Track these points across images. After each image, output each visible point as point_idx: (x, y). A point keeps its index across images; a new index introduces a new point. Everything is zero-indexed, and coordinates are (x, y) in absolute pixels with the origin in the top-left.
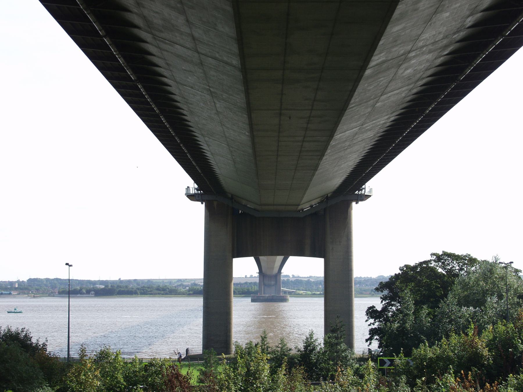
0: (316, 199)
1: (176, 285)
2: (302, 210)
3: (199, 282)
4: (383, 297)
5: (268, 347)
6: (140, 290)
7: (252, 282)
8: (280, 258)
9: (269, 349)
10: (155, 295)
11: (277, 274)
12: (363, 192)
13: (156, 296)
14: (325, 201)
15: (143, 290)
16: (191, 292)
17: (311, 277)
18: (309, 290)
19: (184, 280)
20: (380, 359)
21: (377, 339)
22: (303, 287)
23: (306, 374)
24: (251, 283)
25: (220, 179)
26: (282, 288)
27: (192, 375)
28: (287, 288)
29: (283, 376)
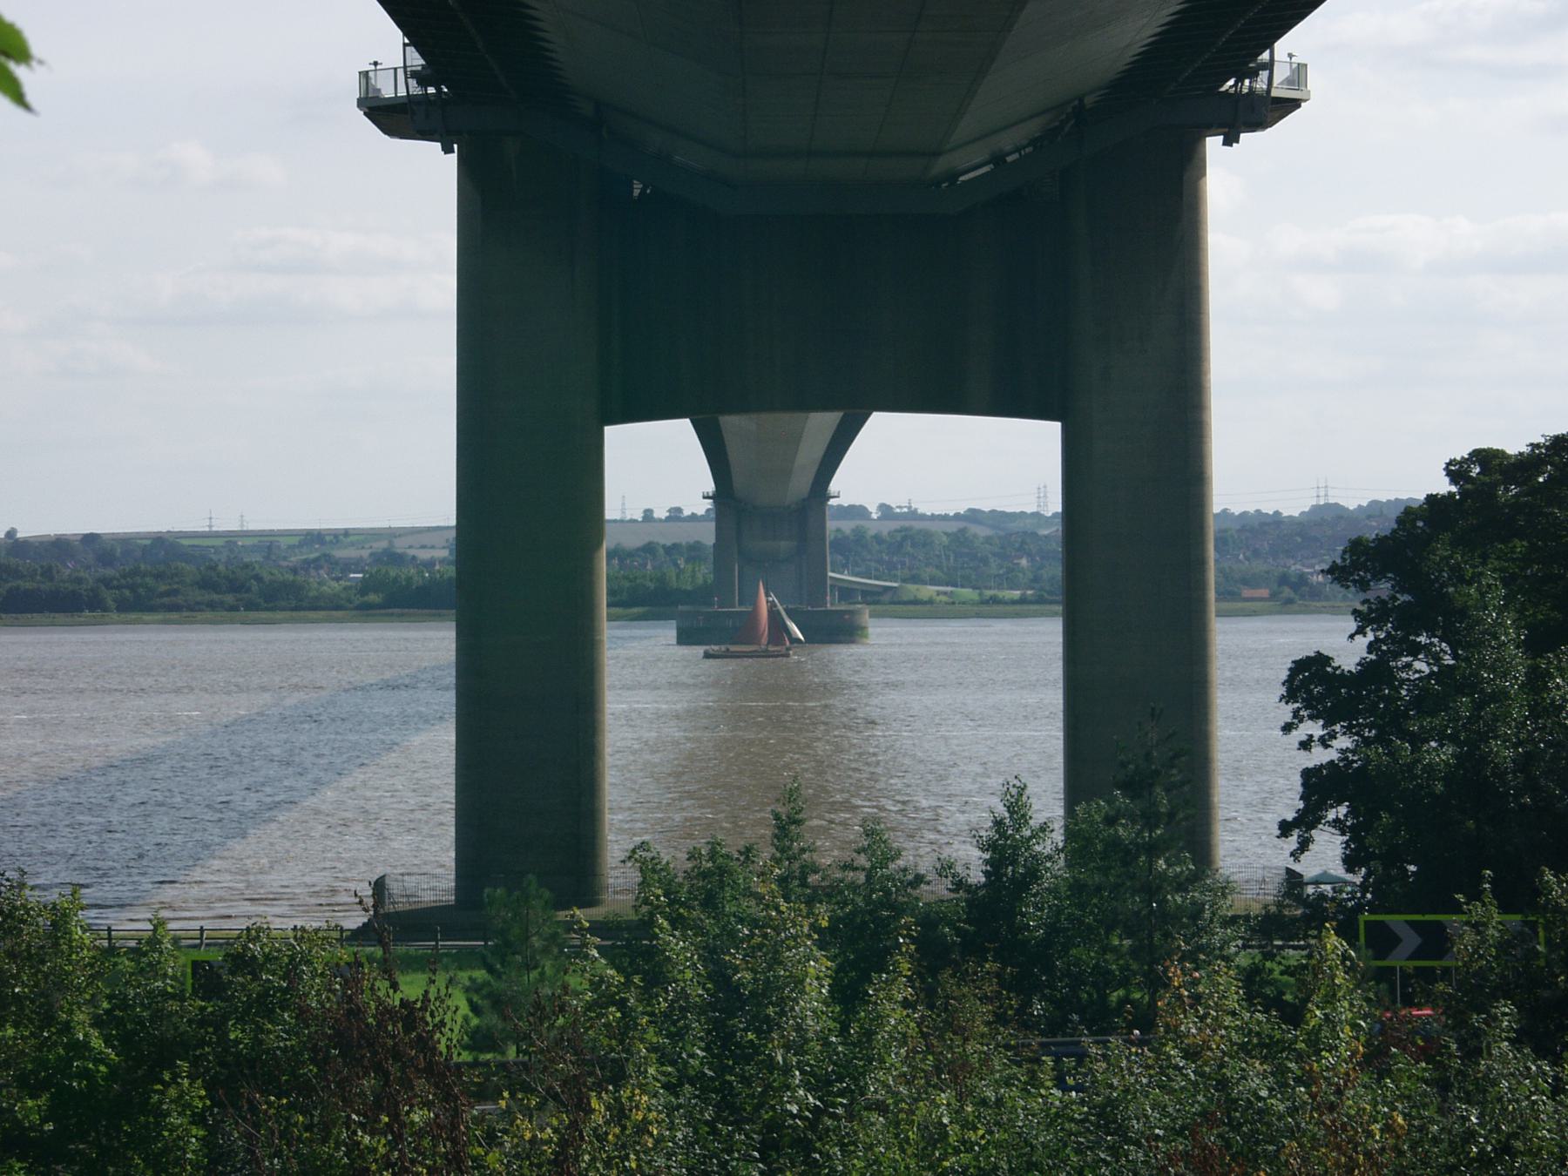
0: (1032, 117)
1: (294, 559)
2: (953, 177)
3: (410, 547)
4: (1364, 608)
5: (808, 869)
6: (118, 588)
7: (677, 541)
8: (823, 423)
9: (813, 879)
10: (192, 610)
11: (804, 500)
12: (1261, 84)
13: (199, 616)
14: (1066, 129)
15: (133, 588)
16: (373, 598)
17: (974, 516)
18: (966, 582)
19: (336, 536)
20: (1366, 922)
21: (1337, 823)
22: (937, 567)
23: (1010, 999)
24: (672, 550)
25: (540, 24)
26: (831, 574)
27: (448, 1007)
28: (857, 569)
29: (900, 1012)
